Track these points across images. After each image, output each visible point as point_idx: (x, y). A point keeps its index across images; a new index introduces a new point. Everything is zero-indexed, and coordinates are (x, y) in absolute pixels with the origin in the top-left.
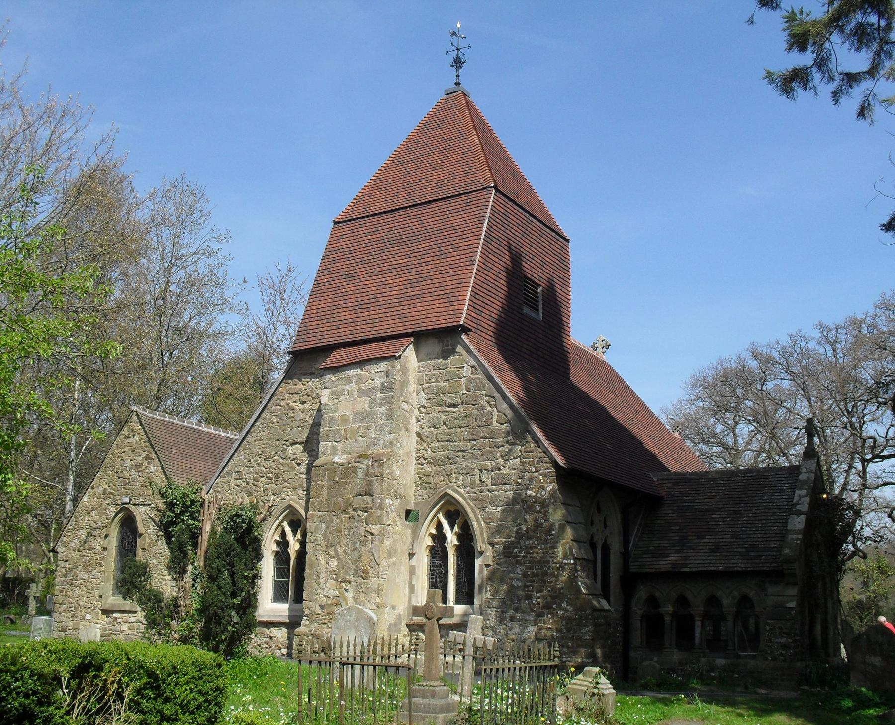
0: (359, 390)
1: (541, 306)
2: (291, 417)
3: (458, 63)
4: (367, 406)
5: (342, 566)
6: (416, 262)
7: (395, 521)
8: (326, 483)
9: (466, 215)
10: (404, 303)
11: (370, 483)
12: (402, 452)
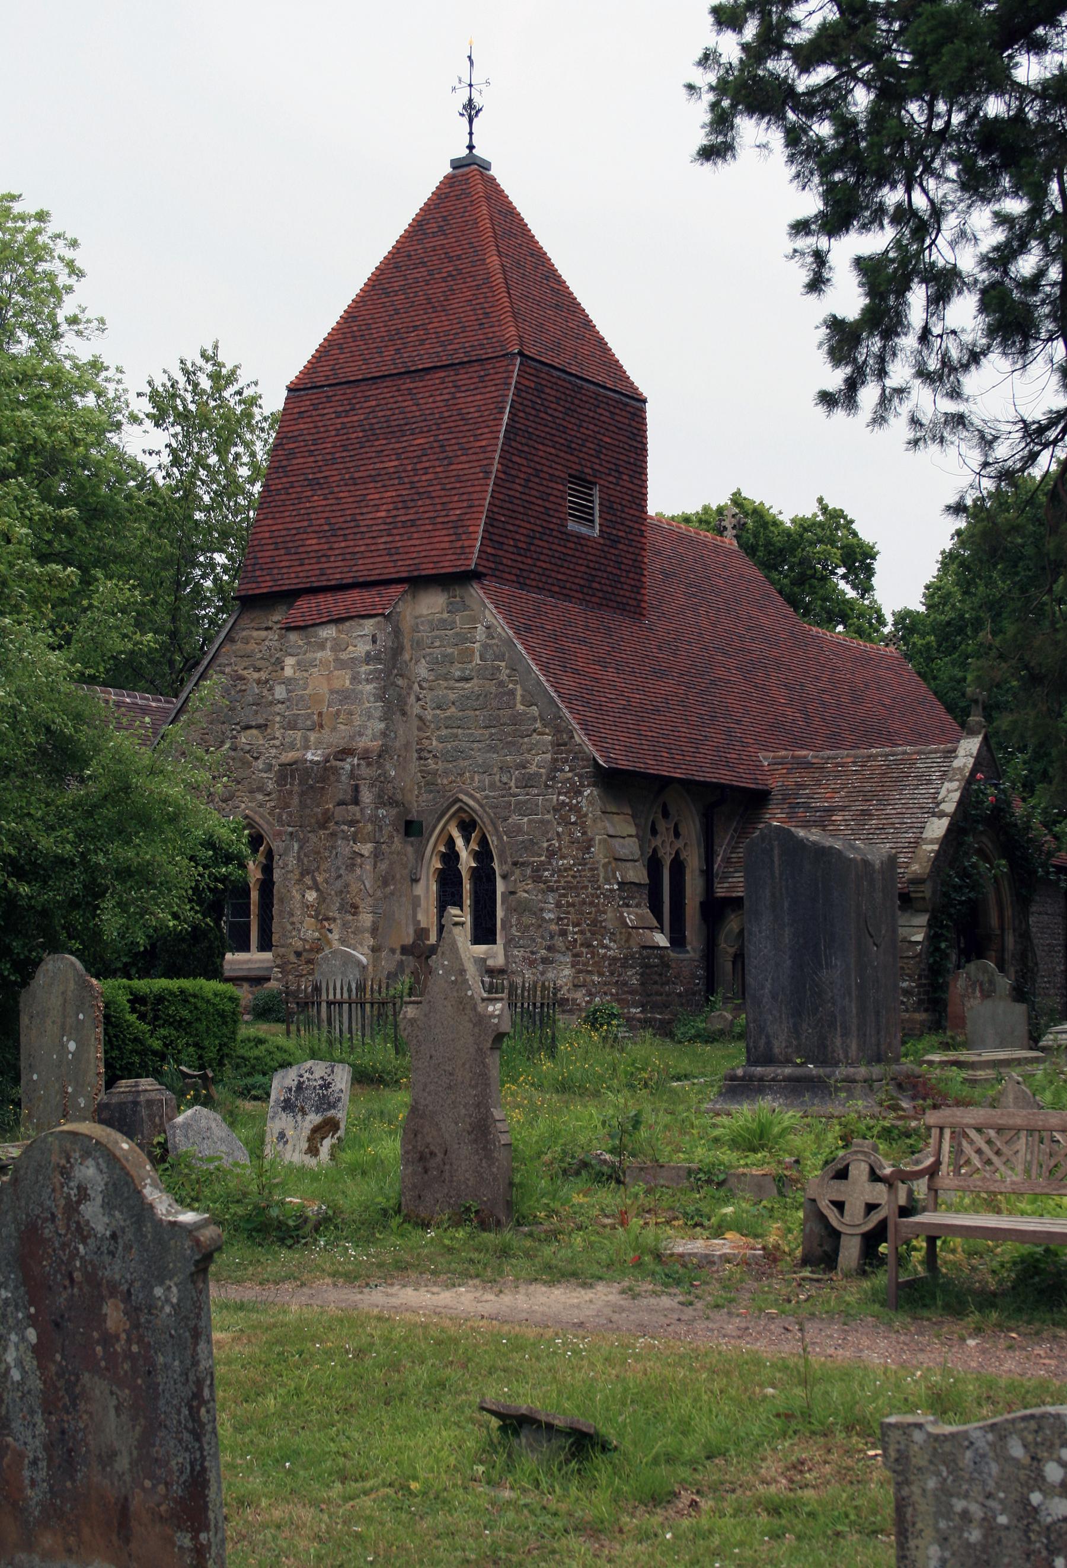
0: (337, 660)
1: (597, 520)
2: (241, 691)
3: (471, 111)
4: (348, 682)
5: (322, 898)
6: (409, 468)
7: (391, 837)
8: (296, 788)
9: (478, 397)
10: (395, 532)
11: (356, 789)
12: (397, 744)
